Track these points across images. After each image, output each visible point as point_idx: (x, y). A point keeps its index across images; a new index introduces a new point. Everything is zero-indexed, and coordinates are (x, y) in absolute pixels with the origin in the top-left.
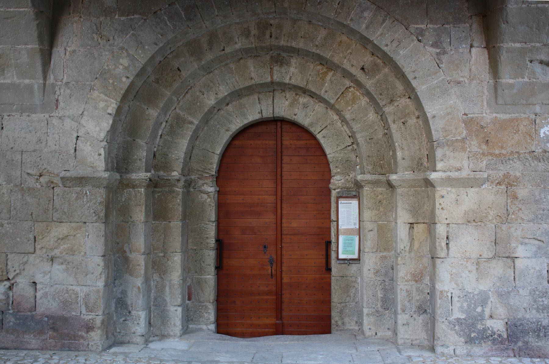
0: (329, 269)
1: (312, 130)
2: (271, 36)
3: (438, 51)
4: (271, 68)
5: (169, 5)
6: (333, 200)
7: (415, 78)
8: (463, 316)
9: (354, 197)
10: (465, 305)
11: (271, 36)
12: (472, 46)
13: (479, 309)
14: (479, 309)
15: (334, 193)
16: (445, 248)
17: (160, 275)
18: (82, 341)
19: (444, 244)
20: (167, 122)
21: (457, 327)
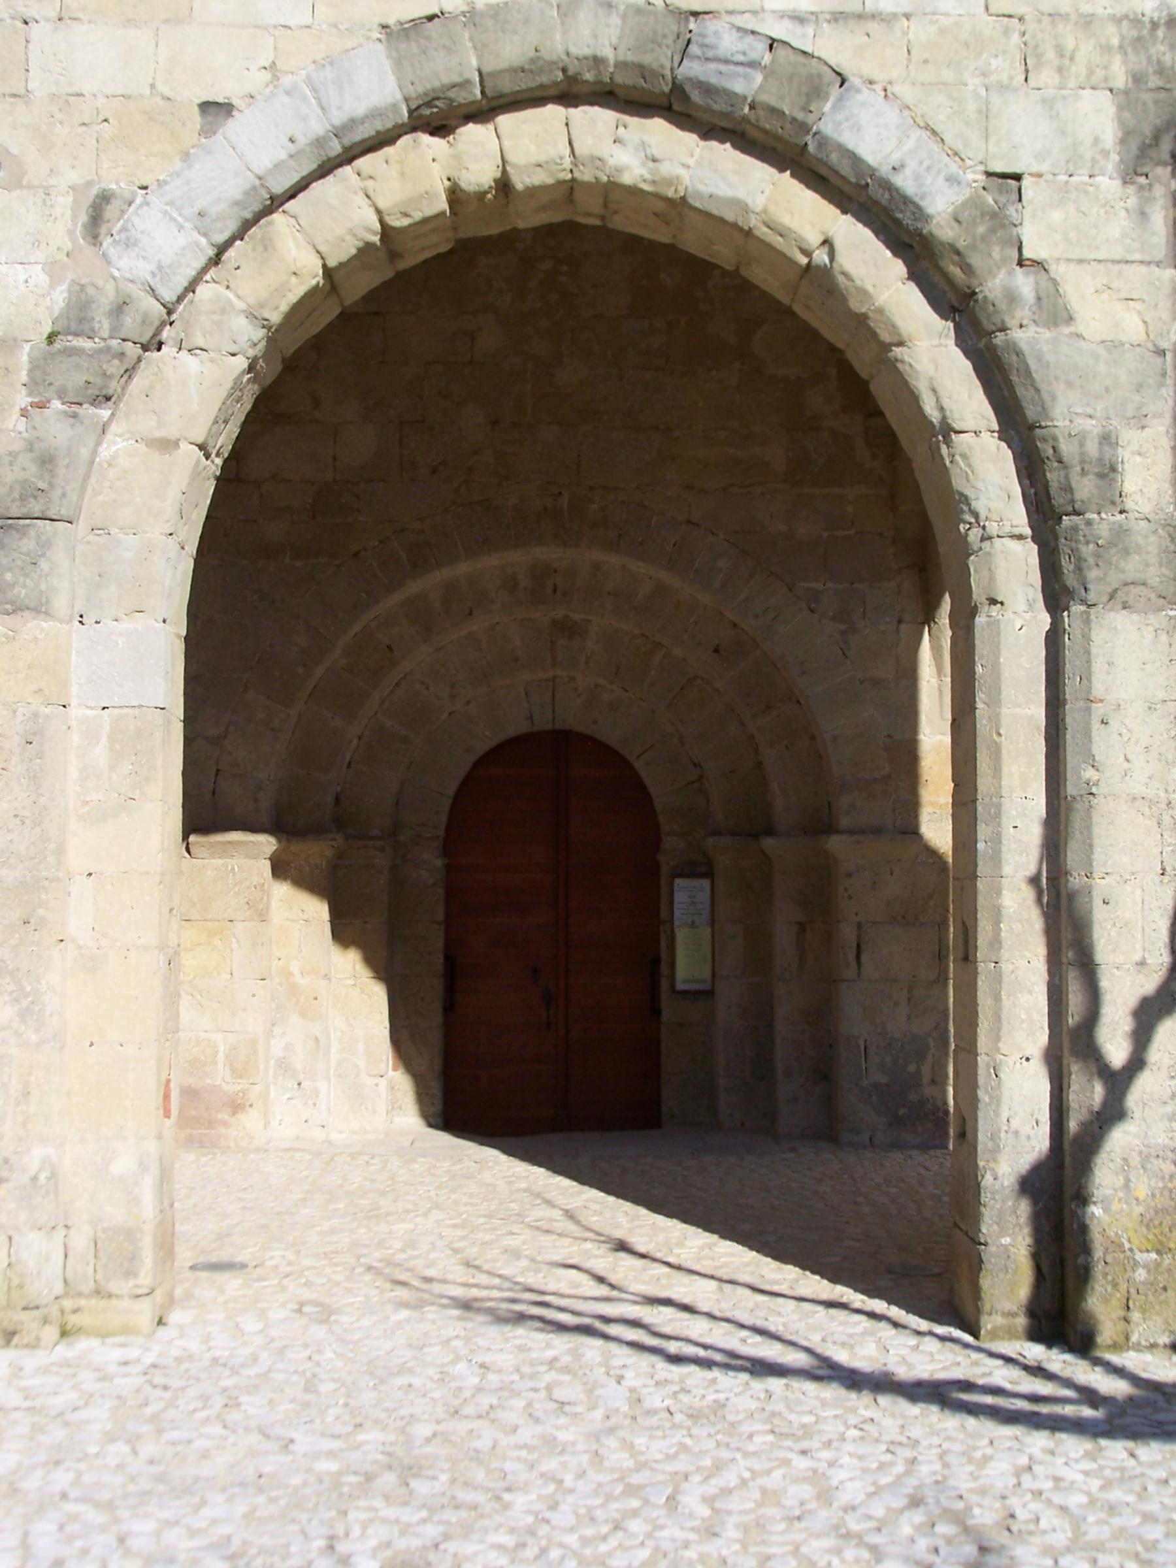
0: (656, 1011)
1: (624, 752)
2: (555, 591)
3: (843, 627)
4: (551, 642)
5: (380, 542)
6: (664, 881)
7: (804, 673)
8: (884, 1079)
9: (702, 876)
10: (888, 1059)
11: (555, 591)
12: (900, 621)
13: (912, 1068)
14: (912, 1068)
15: (665, 870)
16: (854, 963)
17: (347, 1018)
18: (222, 1130)
19: (852, 957)
20: (360, 738)
21: (874, 1099)
